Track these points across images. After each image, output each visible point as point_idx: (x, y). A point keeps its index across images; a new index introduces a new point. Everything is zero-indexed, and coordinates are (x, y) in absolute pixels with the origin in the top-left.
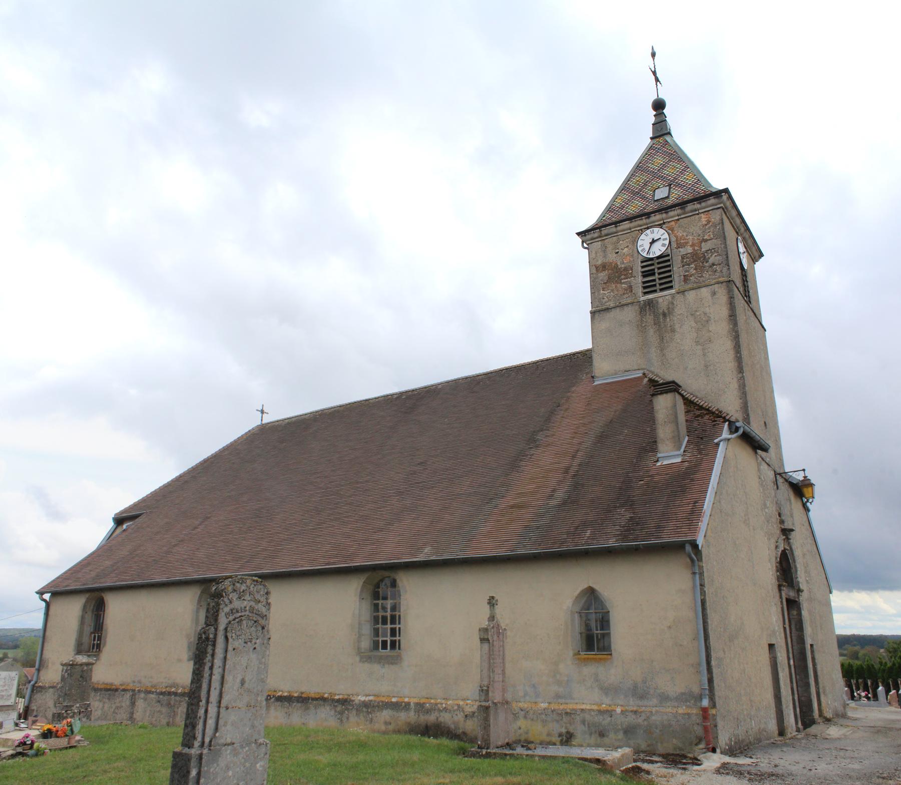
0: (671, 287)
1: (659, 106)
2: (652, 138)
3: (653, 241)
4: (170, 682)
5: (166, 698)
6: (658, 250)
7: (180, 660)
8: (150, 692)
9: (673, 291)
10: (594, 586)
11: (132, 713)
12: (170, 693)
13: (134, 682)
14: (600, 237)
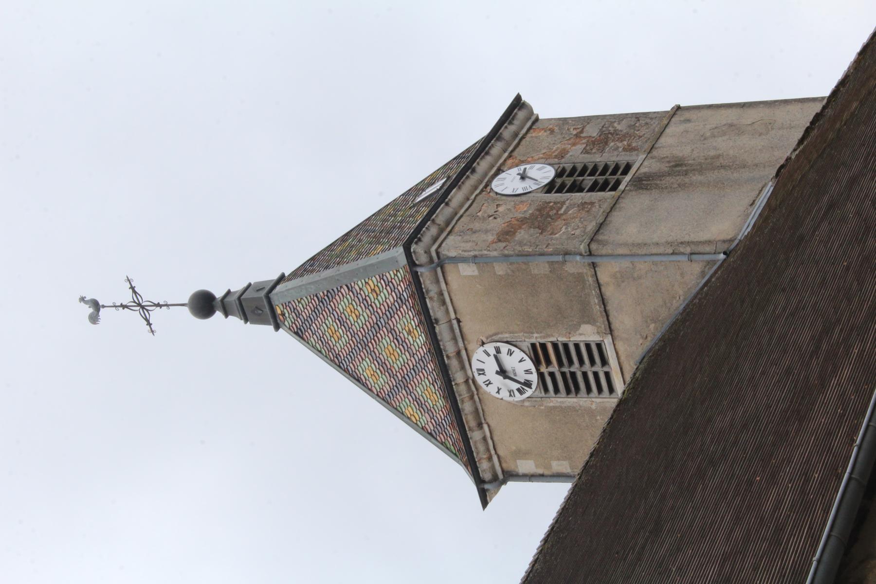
0: (599, 346)
1: (205, 304)
2: (277, 327)
3: (502, 372)
6: (520, 363)
9: (607, 343)
14: (441, 231)
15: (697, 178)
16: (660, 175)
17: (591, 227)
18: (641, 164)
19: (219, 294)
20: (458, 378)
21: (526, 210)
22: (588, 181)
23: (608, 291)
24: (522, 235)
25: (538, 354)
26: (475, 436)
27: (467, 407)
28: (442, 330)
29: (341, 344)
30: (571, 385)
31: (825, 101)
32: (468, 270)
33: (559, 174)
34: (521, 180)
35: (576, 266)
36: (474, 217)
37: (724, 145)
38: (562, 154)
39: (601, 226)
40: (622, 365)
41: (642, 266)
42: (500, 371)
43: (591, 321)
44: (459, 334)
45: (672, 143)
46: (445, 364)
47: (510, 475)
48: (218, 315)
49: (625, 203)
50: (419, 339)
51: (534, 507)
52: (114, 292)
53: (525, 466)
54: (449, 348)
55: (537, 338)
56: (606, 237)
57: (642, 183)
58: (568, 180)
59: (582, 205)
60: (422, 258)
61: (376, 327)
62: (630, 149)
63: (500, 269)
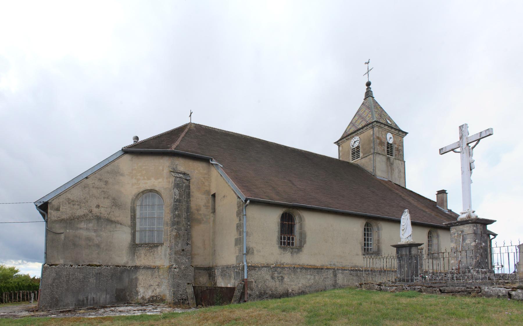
1: (368, 84)
3: (355, 142)
4: (353, 265)
5: (355, 272)
7: (357, 255)
8: (345, 270)
10: (360, 252)
11: (336, 281)
12: (356, 270)
13: (331, 265)
15: (389, 167)
16: (390, 161)
17: (379, 152)
18: (392, 158)
19: (370, 86)
20: (354, 135)
21: (383, 140)
22: (389, 150)
23: (368, 157)
24: (378, 141)
25: (358, 147)
26: (345, 139)
27: (349, 137)
28: (362, 130)
29: (361, 112)
30: (353, 154)
31: (403, 186)
32: (372, 133)
33: (391, 144)
34: (390, 138)
35: (372, 151)
36: (382, 131)
37: (396, 171)
38: (395, 144)
39: (379, 154)
40: (357, 161)
41: (372, 162)
42: (355, 142)
43: (363, 155)
44: (361, 133)
45: (397, 163)
46: (356, 132)
47: (339, 146)
48: (367, 87)
49: (384, 157)
50: (360, 126)
51: (333, 152)
52: (370, 66)
53: (341, 148)
54: (358, 132)
55: (360, 147)
56: (143, 255)
57: (388, 159)
58: (390, 146)
59: (384, 150)
60: (373, 124)
61: (363, 118)
62: (396, 155)
63: (372, 138)
